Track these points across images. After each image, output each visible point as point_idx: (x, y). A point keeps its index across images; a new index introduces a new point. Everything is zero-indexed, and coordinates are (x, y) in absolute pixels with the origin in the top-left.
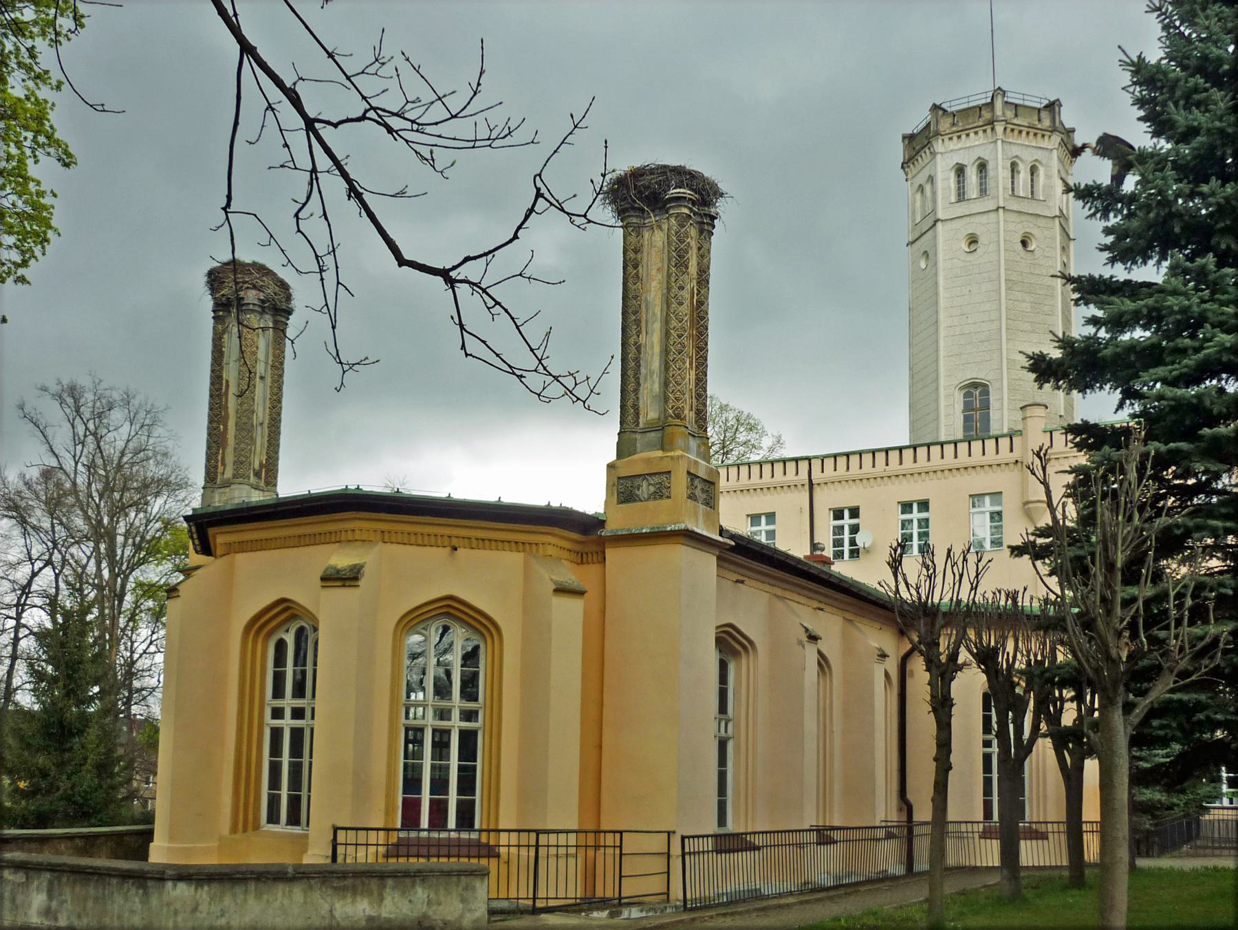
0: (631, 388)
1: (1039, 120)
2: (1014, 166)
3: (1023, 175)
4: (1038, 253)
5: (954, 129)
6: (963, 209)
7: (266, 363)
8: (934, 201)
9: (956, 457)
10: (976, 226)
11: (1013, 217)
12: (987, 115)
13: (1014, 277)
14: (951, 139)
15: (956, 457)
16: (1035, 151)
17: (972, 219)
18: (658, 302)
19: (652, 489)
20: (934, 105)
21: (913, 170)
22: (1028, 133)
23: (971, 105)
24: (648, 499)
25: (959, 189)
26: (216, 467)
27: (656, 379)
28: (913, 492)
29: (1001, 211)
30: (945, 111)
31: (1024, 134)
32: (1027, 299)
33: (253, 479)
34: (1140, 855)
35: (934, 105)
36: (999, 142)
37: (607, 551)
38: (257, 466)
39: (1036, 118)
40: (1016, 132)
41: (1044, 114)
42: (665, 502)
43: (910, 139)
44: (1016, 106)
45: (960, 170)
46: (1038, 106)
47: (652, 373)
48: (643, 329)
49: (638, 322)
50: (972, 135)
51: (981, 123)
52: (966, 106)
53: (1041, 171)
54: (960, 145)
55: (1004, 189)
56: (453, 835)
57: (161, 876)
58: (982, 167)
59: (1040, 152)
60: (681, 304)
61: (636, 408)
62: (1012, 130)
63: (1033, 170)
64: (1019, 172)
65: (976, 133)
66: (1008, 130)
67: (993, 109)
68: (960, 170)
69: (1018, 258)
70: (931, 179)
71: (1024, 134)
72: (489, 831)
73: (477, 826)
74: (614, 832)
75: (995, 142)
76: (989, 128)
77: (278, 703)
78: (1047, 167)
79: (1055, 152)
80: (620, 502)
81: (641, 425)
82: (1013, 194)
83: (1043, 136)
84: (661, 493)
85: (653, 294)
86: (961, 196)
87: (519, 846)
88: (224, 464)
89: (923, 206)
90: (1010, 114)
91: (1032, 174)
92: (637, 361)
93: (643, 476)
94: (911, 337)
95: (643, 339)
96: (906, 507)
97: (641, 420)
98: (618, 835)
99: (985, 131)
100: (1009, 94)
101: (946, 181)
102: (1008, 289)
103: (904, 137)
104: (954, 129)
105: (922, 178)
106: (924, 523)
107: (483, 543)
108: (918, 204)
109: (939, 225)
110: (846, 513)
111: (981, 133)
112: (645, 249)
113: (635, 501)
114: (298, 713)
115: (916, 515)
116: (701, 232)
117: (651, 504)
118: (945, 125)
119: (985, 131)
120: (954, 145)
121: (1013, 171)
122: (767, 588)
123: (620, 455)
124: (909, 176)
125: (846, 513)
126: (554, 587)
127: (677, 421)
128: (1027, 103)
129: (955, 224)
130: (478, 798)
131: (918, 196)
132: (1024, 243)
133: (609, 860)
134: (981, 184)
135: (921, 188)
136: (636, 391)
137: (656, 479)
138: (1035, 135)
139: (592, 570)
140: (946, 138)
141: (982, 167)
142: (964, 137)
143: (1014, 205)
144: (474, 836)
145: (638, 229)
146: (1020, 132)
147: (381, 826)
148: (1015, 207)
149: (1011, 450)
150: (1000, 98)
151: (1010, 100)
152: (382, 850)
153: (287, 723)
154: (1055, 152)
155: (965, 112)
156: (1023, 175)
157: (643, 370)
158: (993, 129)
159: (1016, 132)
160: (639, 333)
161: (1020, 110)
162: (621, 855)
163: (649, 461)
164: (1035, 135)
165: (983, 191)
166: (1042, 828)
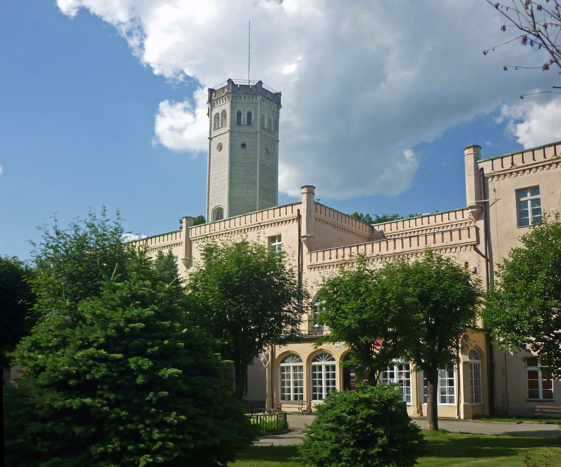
2: (239, 114)
3: (244, 117)
13: (261, 162)
96: (520, 192)
156: (244, 117)
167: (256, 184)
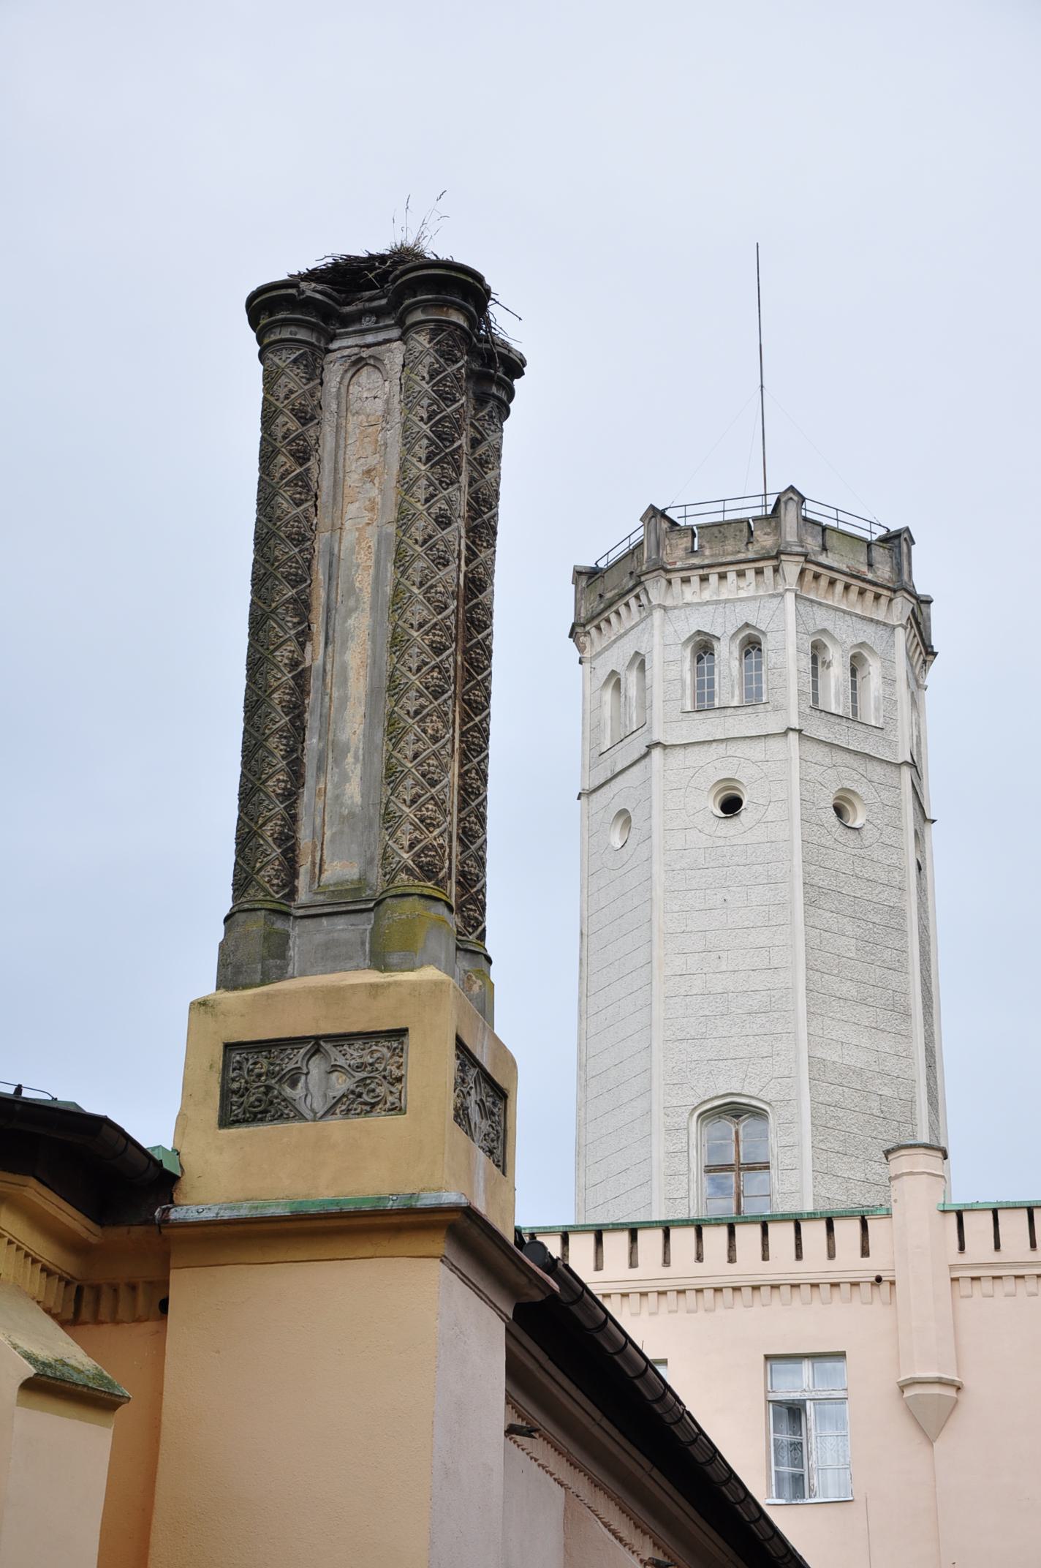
0: (276, 784)
1: (870, 565)
2: (817, 653)
3: (837, 673)
4: (868, 833)
5: (696, 561)
6: (707, 727)
8: (644, 705)
9: (732, 1259)
10: (744, 768)
11: (819, 753)
12: (765, 540)
13: (821, 879)
14: (686, 581)
15: (732, 1259)
16: (859, 624)
17: (733, 749)
18: (365, 559)
19: (341, 1084)
20: (652, 507)
21: (596, 641)
22: (847, 587)
23: (730, 516)
24: (330, 1111)
25: (700, 685)
27: (354, 770)
29: (793, 737)
30: (674, 524)
31: (839, 587)
32: (850, 928)
35: (652, 507)
36: (790, 597)
37: (175, 1276)
39: (863, 558)
40: (824, 582)
41: (878, 553)
42: (380, 1122)
43: (588, 577)
44: (824, 529)
45: (703, 648)
46: (867, 536)
47: (345, 750)
48: (318, 628)
49: (302, 607)
50: (732, 576)
51: (751, 555)
52: (718, 518)
53: (874, 668)
54: (707, 595)
55: (800, 692)
58: (752, 645)
59: (871, 629)
60: (443, 562)
61: (288, 844)
62: (817, 577)
63: (856, 665)
64: (828, 665)
65: (741, 574)
66: (809, 577)
67: (778, 529)
68: (703, 648)
69: (830, 843)
70: (639, 662)
71: (839, 587)
75: (782, 595)
76: (768, 566)
78: (888, 662)
79: (900, 631)
80: (226, 1120)
81: (303, 897)
82: (815, 708)
83: (877, 597)
84: (372, 1095)
85: (349, 537)
86: (704, 701)
89: (617, 718)
90: (813, 544)
91: (854, 672)
92: (297, 711)
93: (316, 1044)
94: (584, 995)
95: (314, 655)
97: (302, 882)
99: (759, 572)
100: (808, 505)
101: (671, 668)
102: (809, 903)
103: (578, 573)
104: (696, 561)
105: (617, 658)
108: (607, 711)
109: (656, 753)
111: (750, 574)
112: (329, 418)
113: (281, 1117)
116: (481, 400)
117: (337, 1127)
118: (675, 553)
119: (759, 572)
120: (690, 593)
121: (814, 659)
122: (563, 1470)
123: (230, 975)
124: (587, 655)
126: (31, 1371)
127: (429, 887)
128: (842, 527)
129: (694, 755)
131: (608, 694)
132: (839, 811)
134: (749, 680)
135: (614, 680)
136: (291, 796)
137: (355, 1054)
138: (862, 592)
139: (127, 1341)
140: (676, 577)
141: (752, 645)
142: (714, 579)
143: (819, 729)
145: (312, 363)
146: (832, 582)
148: (823, 734)
149: (865, 1252)
150: (792, 507)
151: (809, 515)
154: (900, 631)
155: (717, 530)
156: (837, 673)
157: (312, 741)
158: (776, 570)
159: (824, 582)
160: (304, 637)
161: (832, 540)
163: (335, 995)
164: (862, 592)
165: (753, 696)
167: (907, 1015)
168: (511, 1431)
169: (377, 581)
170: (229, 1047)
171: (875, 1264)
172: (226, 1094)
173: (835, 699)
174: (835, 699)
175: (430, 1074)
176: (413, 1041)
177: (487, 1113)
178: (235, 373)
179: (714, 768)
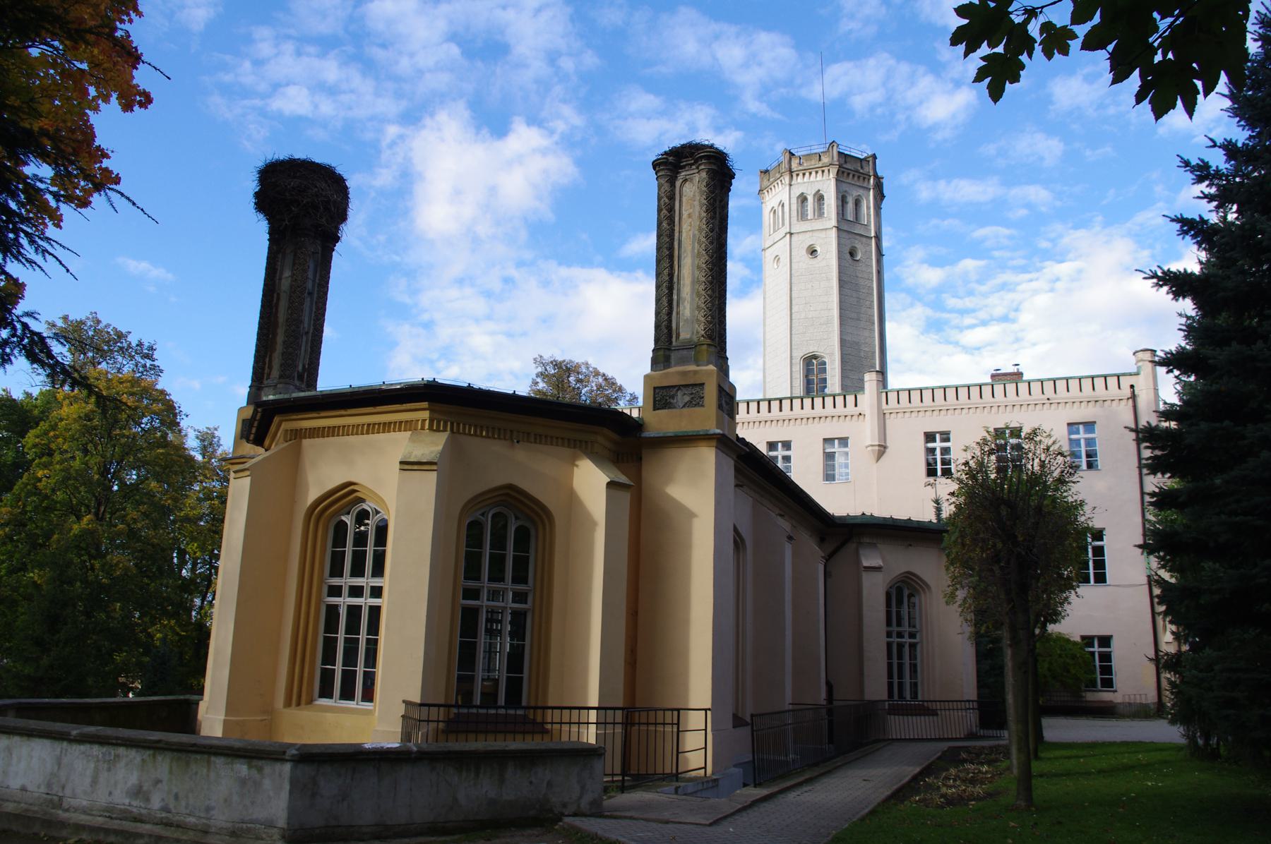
3: (850, 206)
7: (314, 281)
17: (816, 234)
19: (687, 399)
26: (263, 369)
28: (936, 424)
33: (297, 383)
34: (185, 717)
38: (300, 368)
42: (697, 409)
45: (803, 199)
56: (502, 711)
57: (212, 750)
72: (535, 708)
73: (524, 704)
74: (672, 710)
76: (826, 169)
77: (335, 581)
84: (696, 401)
87: (579, 723)
88: (270, 368)
93: (679, 387)
96: (930, 437)
98: (675, 713)
106: (946, 451)
107: (371, 429)
110: (930, 445)
114: (912, 635)
115: (938, 445)
117: (686, 410)
125: (930, 445)
130: (525, 675)
133: (668, 737)
144: (520, 712)
145: (672, 181)
147: (442, 702)
152: (441, 725)
153: (907, 640)
156: (850, 206)
162: (678, 731)
163: (685, 373)
166: (933, 706)
168: (736, 486)
169: (693, 248)
170: (655, 388)
171: (859, 409)
172: (655, 401)
173: (850, 216)
174: (850, 216)
175: (711, 394)
176: (706, 387)
177: (727, 403)
178: (649, 184)
179: (808, 240)
